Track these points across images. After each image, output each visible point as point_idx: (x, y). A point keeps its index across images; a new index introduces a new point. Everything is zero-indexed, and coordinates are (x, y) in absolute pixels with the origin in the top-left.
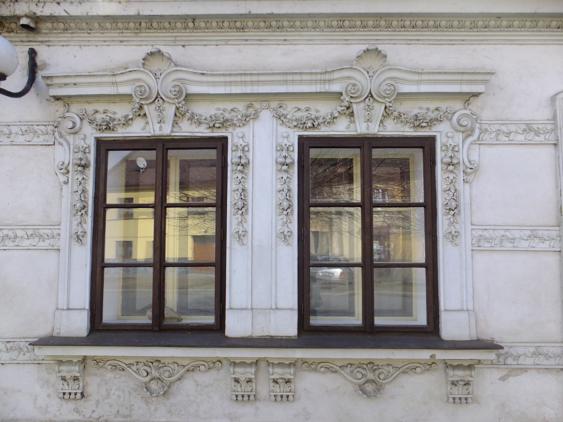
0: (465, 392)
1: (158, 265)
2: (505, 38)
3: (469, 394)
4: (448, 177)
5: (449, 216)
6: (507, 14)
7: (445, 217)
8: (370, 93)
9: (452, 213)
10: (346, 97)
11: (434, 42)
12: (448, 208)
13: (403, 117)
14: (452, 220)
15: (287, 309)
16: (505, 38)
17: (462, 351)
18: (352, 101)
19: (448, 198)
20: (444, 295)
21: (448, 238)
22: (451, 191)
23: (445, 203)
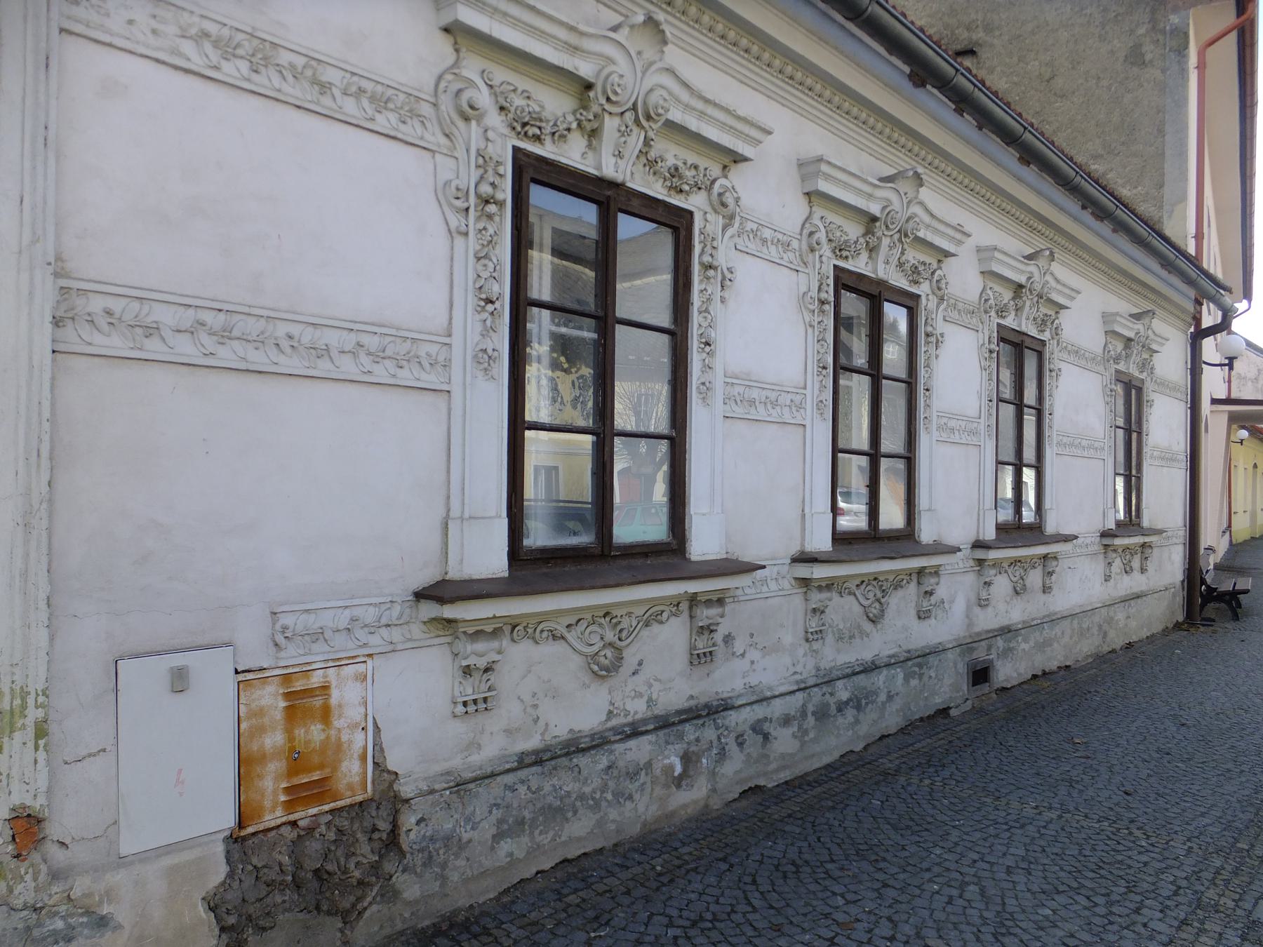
0: (484, 687)
1: (610, 321)
2: (957, 196)
3: (490, 689)
4: (485, 229)
5: (486, 315)
6: (988, 180)
7: (478, 317)
8: (635, 104)
9: (490, 307)
10: (600, 96)
11: (845, 137)
12: (484, 296)
13: (660, 164)
14: (488, 323)
15: (65, 353)
16: (957, 196)
17: (472, 602)
18: (607, 107)
19: (485, 275)
20: (51, 459)
21: (481, 361)
22: (491, 260)
23: (477, 286)
